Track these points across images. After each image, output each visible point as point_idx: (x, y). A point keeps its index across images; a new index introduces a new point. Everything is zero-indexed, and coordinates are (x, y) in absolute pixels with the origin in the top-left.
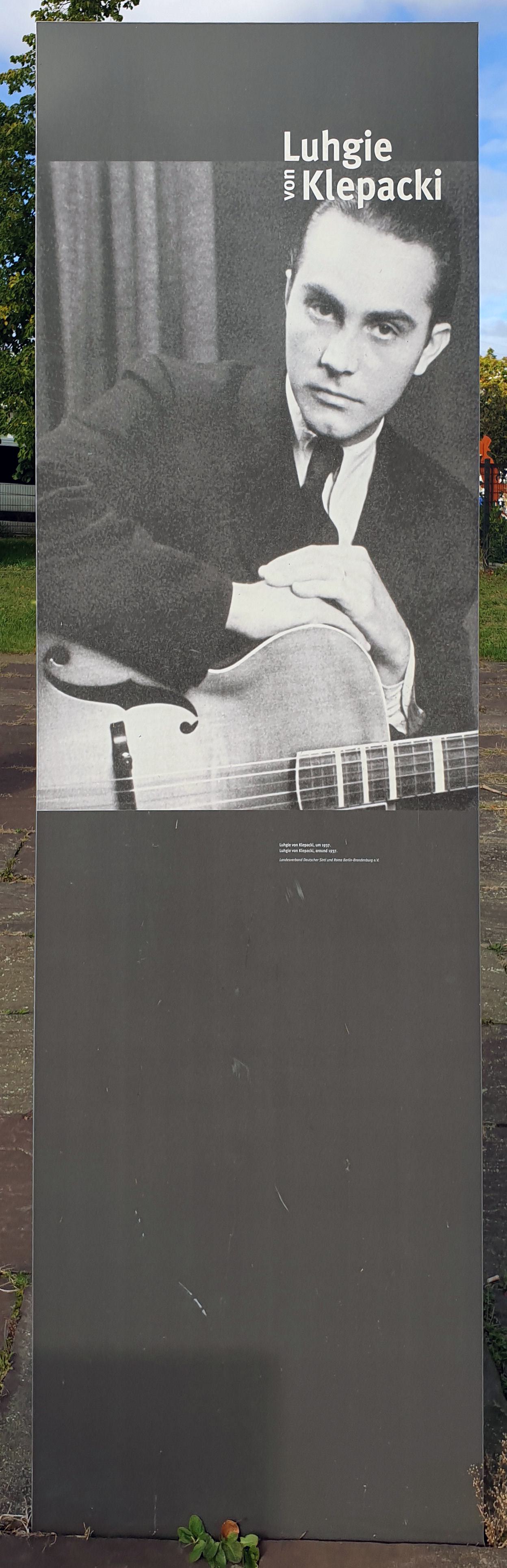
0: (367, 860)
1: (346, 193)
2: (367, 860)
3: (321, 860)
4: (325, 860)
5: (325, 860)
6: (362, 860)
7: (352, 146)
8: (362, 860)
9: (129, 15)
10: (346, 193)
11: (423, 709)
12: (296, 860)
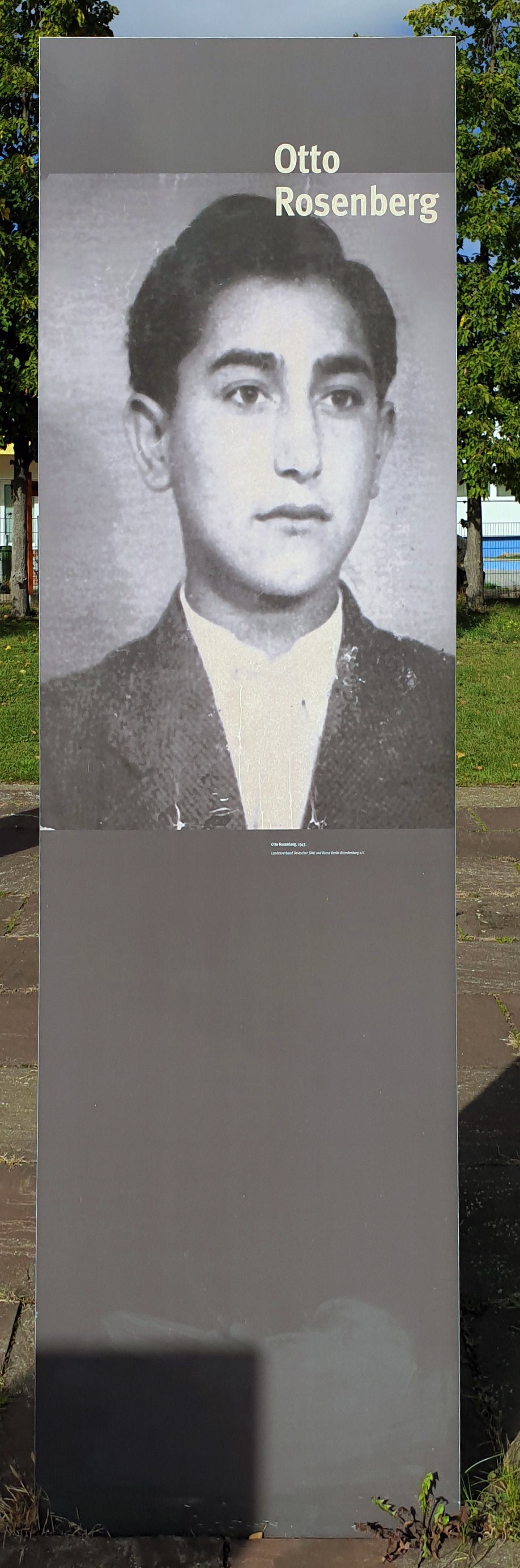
0: (353, 853)
2: (353, 853)
5: (313, 853)
6: (349, 853)
7: (428, 201)
8: (349, 853)
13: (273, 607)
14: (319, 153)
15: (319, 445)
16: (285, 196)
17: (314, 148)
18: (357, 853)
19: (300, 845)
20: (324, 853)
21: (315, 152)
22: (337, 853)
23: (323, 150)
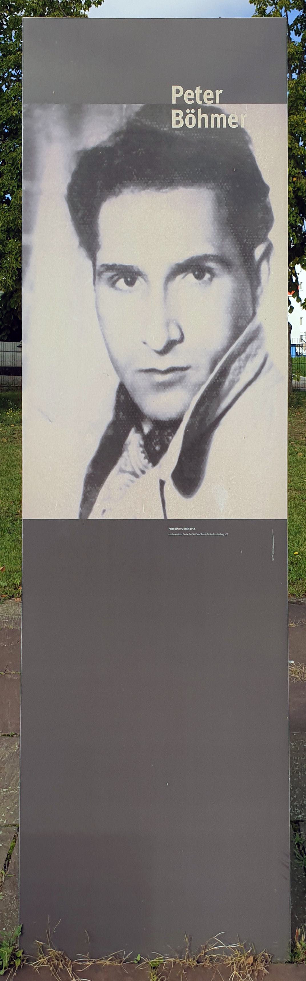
0: (220, 534)
1: (209, 100)
2: (220, 534)
3: (193, 534)
4: (195, 534)
5: (195, 534)
6: (218, 534)
8: (218, 534)
9: (93, 13)
10: (209, 100)
11: (292, 660)
12: (178, 534)
13: (222, 369)
14: (201, 91)
15: (269, 274)
16: (178, 91)
17: (198, 88)
18: (223, 534)
19: (192, 529)
20: (202, 534)
21: (198, 90)
22: (211, 534)
23: (203, 89)
